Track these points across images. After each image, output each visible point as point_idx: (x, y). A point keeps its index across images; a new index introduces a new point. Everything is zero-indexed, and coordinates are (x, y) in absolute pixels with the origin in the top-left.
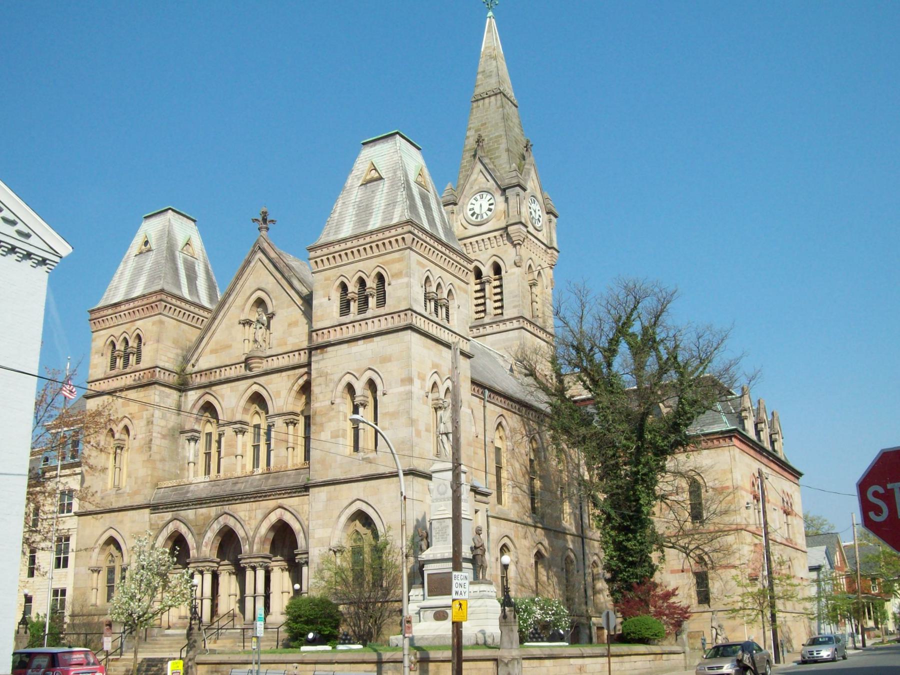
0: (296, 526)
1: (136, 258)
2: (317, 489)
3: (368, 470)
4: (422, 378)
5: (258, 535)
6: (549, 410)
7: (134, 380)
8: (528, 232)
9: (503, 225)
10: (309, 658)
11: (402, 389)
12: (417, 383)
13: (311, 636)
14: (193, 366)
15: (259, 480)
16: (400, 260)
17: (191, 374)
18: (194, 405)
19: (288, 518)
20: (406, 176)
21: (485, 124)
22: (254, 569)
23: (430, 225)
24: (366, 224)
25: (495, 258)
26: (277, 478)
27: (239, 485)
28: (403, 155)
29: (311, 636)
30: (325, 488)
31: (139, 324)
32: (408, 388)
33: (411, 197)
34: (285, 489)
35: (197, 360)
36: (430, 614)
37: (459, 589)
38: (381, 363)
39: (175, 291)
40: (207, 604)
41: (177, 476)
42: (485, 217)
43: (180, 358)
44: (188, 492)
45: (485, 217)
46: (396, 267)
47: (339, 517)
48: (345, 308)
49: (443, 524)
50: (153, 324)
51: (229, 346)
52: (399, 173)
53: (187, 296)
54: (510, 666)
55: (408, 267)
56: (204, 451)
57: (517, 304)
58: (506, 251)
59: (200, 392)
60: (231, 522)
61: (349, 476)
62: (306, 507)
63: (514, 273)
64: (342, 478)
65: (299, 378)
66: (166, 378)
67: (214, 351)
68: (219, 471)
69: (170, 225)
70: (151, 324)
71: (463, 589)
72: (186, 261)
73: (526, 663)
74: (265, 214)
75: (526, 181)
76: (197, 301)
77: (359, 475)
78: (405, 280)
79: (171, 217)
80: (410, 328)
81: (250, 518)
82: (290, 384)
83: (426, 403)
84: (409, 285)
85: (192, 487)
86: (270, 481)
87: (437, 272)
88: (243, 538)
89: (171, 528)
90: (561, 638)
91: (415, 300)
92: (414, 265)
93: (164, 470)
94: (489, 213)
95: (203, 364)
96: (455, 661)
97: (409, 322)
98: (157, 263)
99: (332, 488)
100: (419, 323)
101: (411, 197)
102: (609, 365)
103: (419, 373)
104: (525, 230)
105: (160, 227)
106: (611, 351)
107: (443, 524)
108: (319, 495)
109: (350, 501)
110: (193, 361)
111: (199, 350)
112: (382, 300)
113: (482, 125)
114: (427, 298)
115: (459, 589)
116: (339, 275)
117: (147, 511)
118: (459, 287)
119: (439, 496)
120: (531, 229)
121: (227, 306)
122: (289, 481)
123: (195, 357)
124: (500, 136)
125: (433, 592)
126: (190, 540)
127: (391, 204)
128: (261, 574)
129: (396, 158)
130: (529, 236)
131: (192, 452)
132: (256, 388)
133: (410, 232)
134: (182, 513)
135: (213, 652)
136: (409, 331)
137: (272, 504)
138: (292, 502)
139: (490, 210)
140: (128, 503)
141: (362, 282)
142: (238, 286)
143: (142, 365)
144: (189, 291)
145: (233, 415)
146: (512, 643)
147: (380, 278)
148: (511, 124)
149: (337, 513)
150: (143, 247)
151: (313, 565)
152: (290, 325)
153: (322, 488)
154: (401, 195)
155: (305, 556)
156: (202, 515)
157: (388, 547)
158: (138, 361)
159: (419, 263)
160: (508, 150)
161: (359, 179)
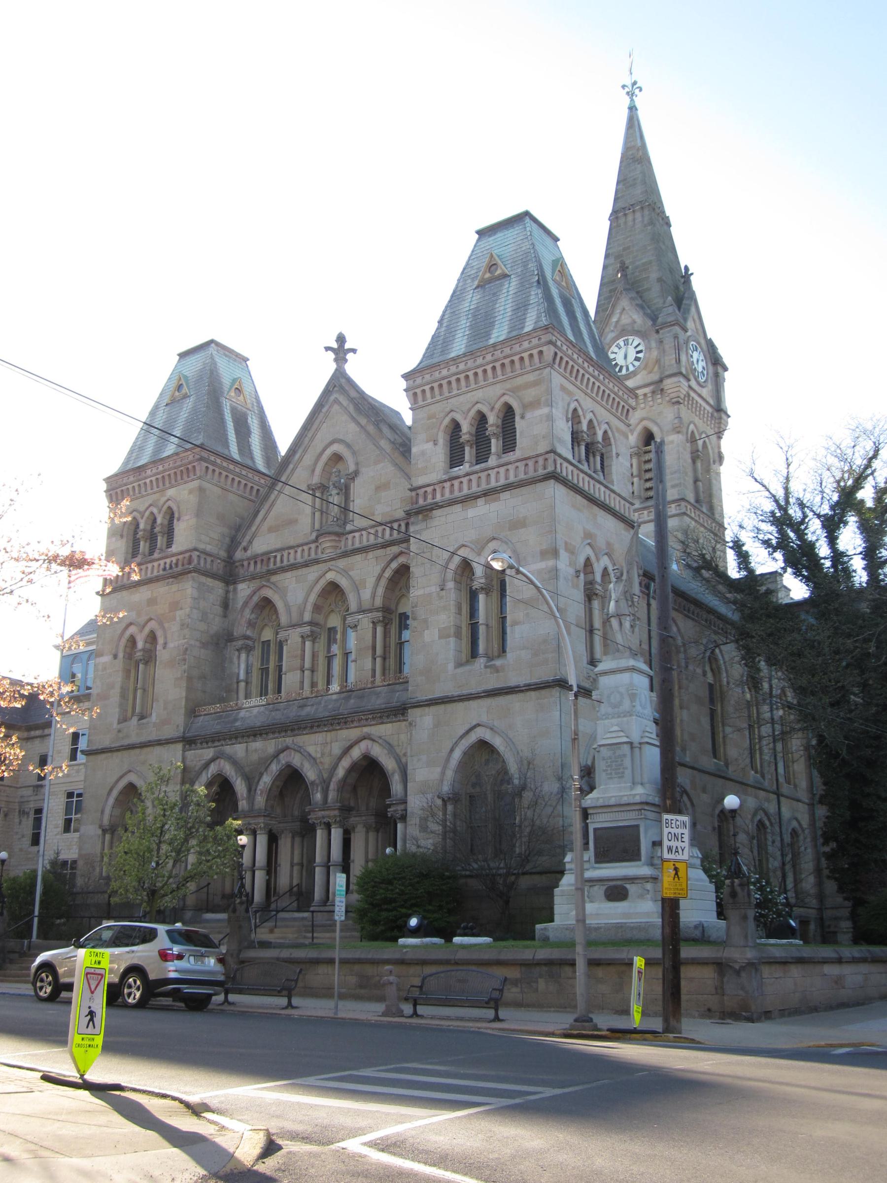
0: (389, 764)
1: (168, 408)
2: (418, 711)
3: (493, 683)
4: (571, 551)
5: (334, 780)
6: (735, 617)
7: (164, 569)
8: (690, 387)
9: (655, 377)
10: (461, 955)
11: (542, 565)
12: (564, 555)
13: (414, 922)
14: (245, 549)
15: (336, 700)
16: (535, 384)
17: (243, 560)
18: (246, 604)
19: (377, 752)
20: (540, 268)
21: (629, 248)
22: (328, 826)
23: (574, 335)
24: (488, 335)
25: (646, 423)
26: (361, 697)
27: (308, 709)
28: (536, 243)
29: (414, 922)
30: (433, 709)
31: (171, 492)
32: (551, 563)
33: (548, 297)
34: (372, 712)
35: (250, 542)
36: (599, 891)
37: (674, 844)
38: (510, 530)
39: (220, 449)
40: (260, 877)
41: (222, 700)
42: (631, 369)
43: (227, 540)
44: (236, 720)
45: (631, 369)
46: (530, 394)
47: (452, 750)
48: (455, 458)
49: (618, 752)
50: (191, 492)
51: (296, 521)
52: (532, 266)
53: (236, 455)
54: (743, 974)
55: (549, 392)
56: (259, 666)
57: (677, 482)
58: (660, 413)
59: (254, 585)
60: (296, 760)
61: (465, 692)
62: (403, 737)
63: (672, 442)
64: (456, 694)
65: (392, 560)
66: (208, 566)
67: (271, 530)
68: (279, 691)
69: (214, 363)
70: (186, 492)
71: (679, 844)
72: (234, 411)
73: (766, 971)
74: (341, 339)
75: (685, 320)
76: (249, 463)
77: (480, 689)
78: (545, 410)
79: (215, 353)
80: (554, 476)
81: (323, 754)
82: (378, 569)
83: (575, 586)
84: (550, 418)
85: (242, 713)
86: (352, 701)
87: (587, 403)
88: (313, 783)
89: (213, 769)
90: (789, 933)
91: (560, 440)
92: (557, 392)
93: (204, 692)
94: (637, 364)
95: (260, 546)
96: (668, 963)
97: (550, 468)
98: (194, 411)
99: (440, 708)
100: (567, 470)
101: (548, 297)
102: (832, 540)
103: (566, 543)
104: (686, 384)
105: (199, 366)
106: (832, 525)
107: (618, 752)
108: (424, 719)
109: (467, 727)
110: (244, 544)
111: (254, 528)
112: (509, 444)
113: (624, 249)
114: (576, 438)
115: (674, 844)
116: (448, 409)
117: (179, 746)
118: (618, 430)
119: (610, 710)
120: (693, 383)
121: (291, 466)
122: (378, 702)
123: (248, 538)
124: (650, 262)
125: (604, 856)
126: (240, 787)
127: (521, 308)
128: (337, 834)
129: (526, 245)
130: (692, 394)
131: (243, 666)
132: (330, 576)
133: (550, 342)
134: (228, 749)
135: (264, 945)
136: (552, 481)
137: (353, 733)
138: (385, 730)
139: (637, 359)
140: (153, 737)
141: (482, 419)
142: (307, 440)
143: (175, 549)
144: (239, 450)
145: (301, 615)
146: (746, 937)
147: (508, 413)
148: (663, 247)
149: (448, 745)
150: (177, 394)
151: (413, 821)
152: (378, 488)
153: (427, 709)
154: (535, 295)
155: (402, 807)
156: (256, 750)
157: (528, 795)
158: (169, 544)
159: (563, 388)
160: (660, 280)
161: (473, 279)
